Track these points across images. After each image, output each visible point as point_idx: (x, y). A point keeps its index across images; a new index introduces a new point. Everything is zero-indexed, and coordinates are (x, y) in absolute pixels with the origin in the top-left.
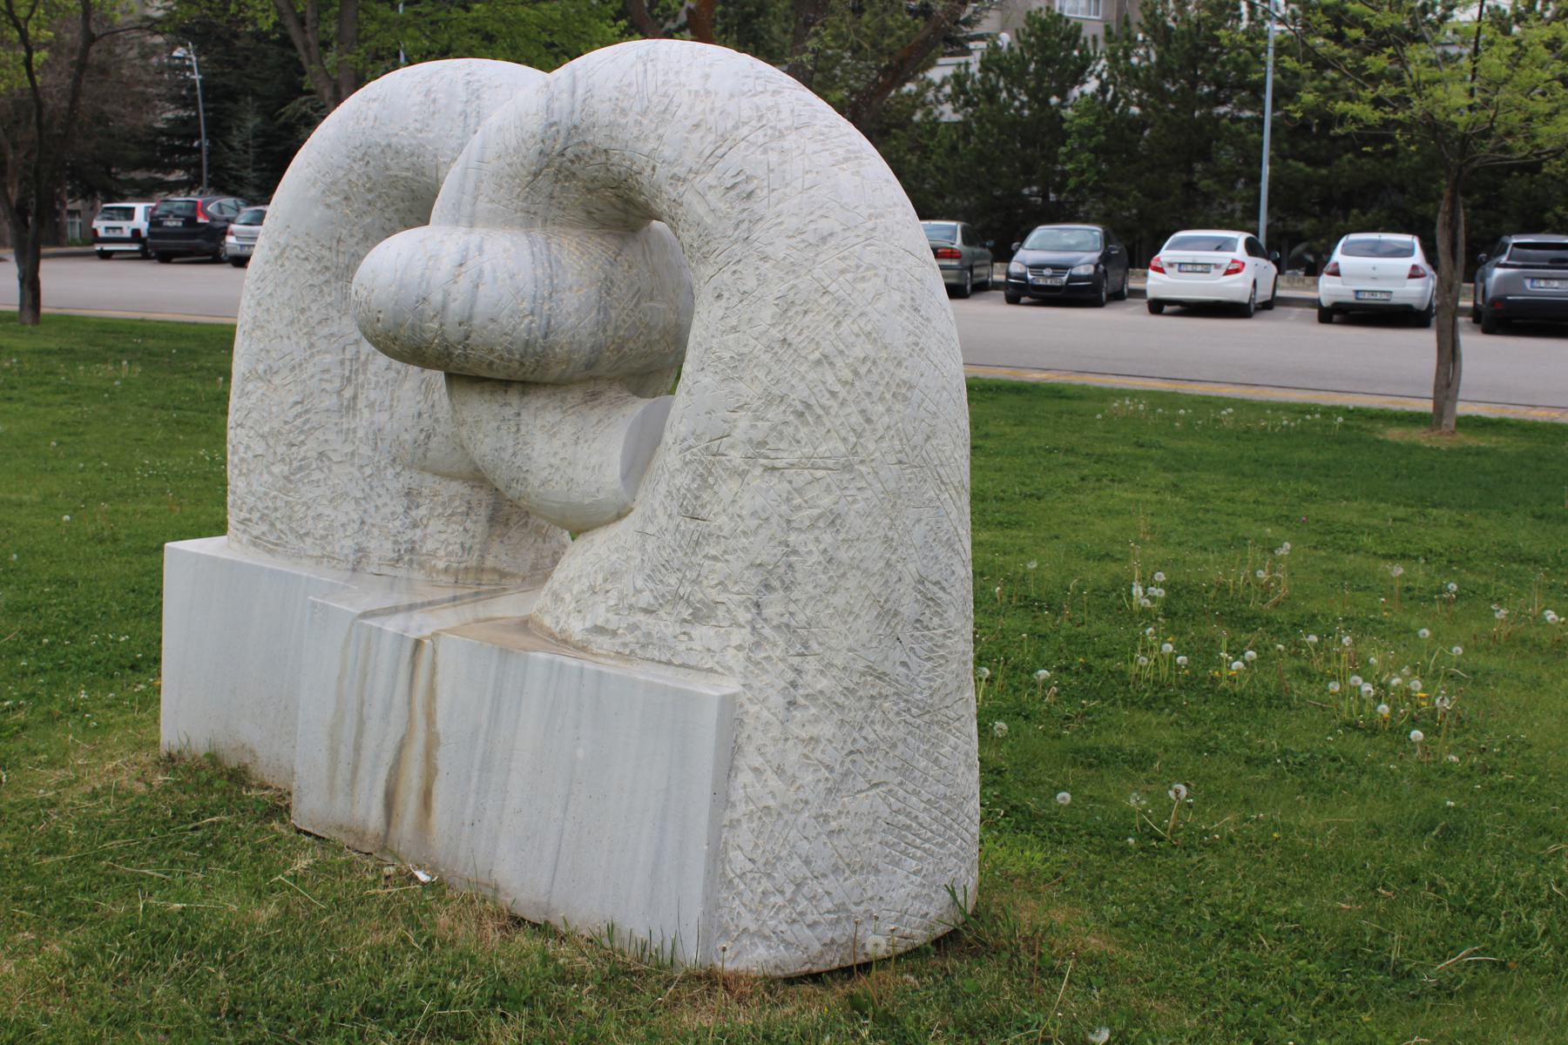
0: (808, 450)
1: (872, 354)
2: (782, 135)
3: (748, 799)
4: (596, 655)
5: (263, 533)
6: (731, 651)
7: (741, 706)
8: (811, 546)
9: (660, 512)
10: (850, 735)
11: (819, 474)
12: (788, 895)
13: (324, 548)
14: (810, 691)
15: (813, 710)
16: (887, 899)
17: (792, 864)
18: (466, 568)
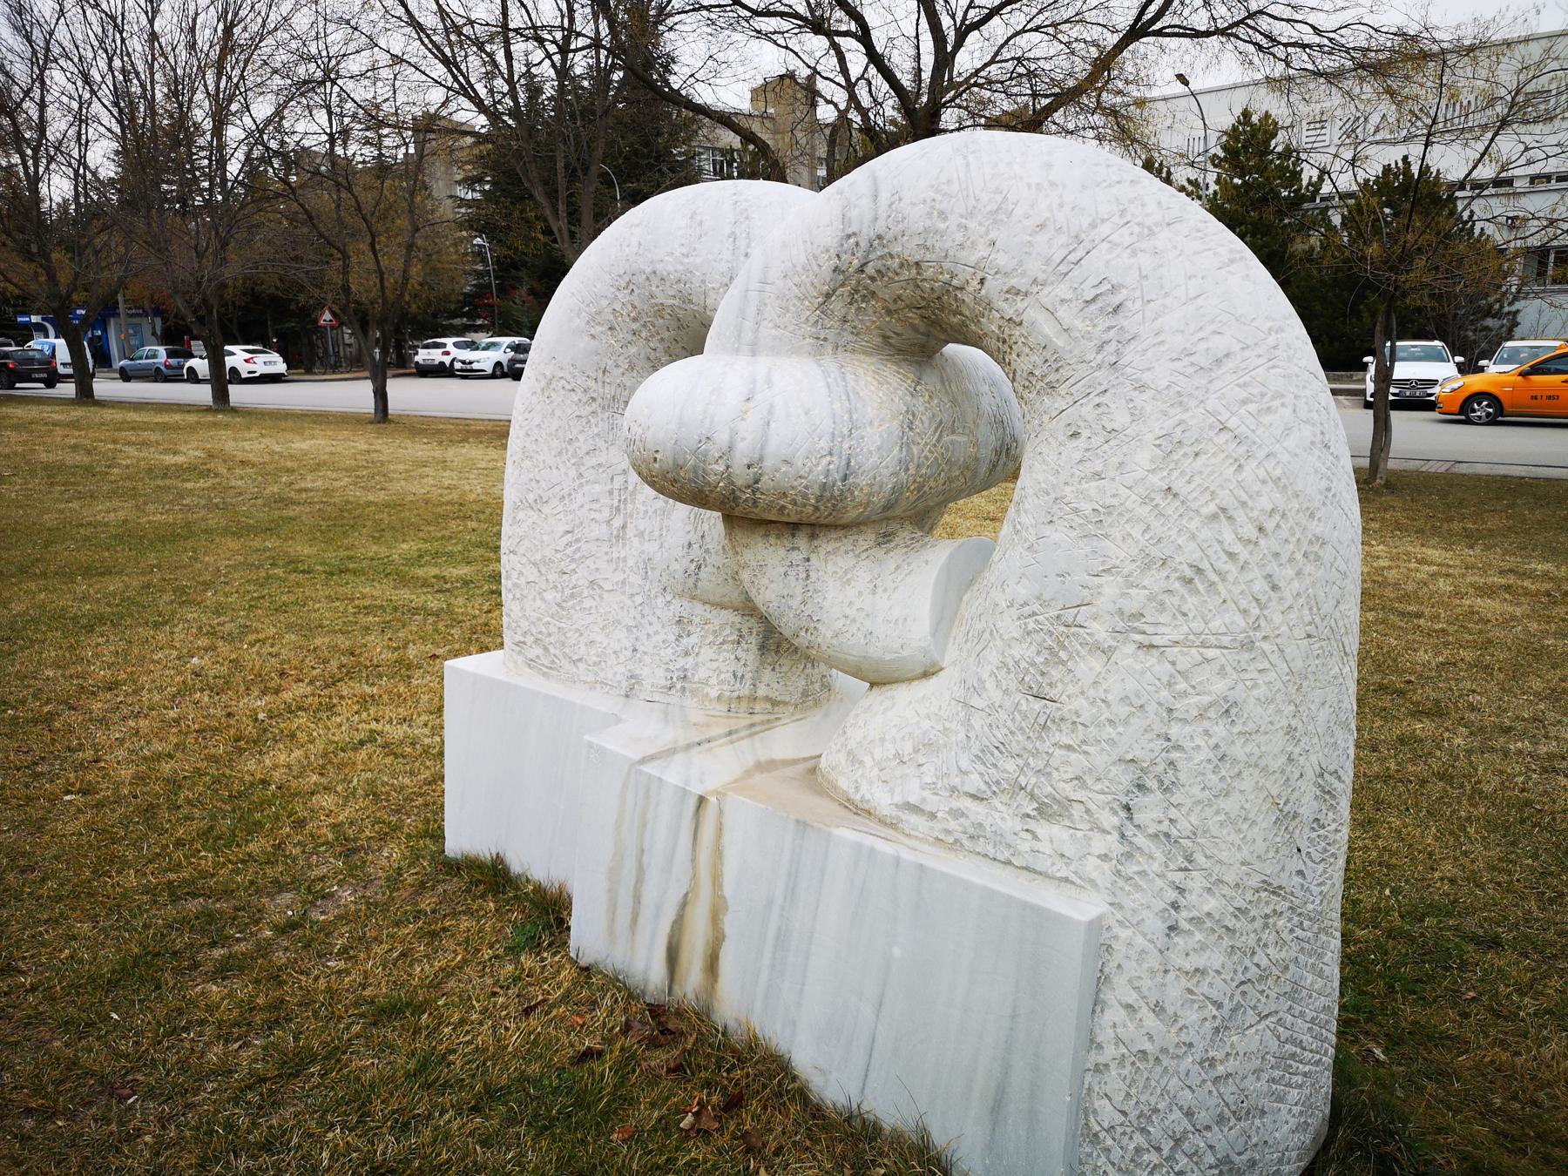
0: (1197, 625)
1: (1282, 506)
2: (1151, 233)
3: (1119, 1040)
4: (909, 836)
5: (538, 657)
6: (1092, 861)
7: (1109, 928)
8: (1198, 741)
9: (990, 684)
10: (1241, 963)
11: (1211, 653)
12: (1165, 1153)
13: (596, 674)
14: (1195, 913)
15: (1198, 936)
16: (1271, 1142)
17: (1172, 1117)
18: (739, 697)
